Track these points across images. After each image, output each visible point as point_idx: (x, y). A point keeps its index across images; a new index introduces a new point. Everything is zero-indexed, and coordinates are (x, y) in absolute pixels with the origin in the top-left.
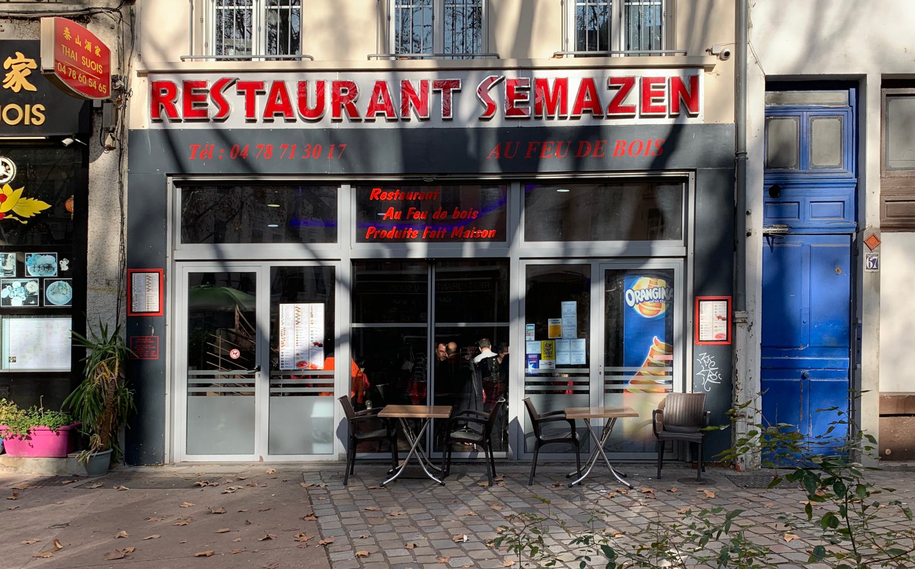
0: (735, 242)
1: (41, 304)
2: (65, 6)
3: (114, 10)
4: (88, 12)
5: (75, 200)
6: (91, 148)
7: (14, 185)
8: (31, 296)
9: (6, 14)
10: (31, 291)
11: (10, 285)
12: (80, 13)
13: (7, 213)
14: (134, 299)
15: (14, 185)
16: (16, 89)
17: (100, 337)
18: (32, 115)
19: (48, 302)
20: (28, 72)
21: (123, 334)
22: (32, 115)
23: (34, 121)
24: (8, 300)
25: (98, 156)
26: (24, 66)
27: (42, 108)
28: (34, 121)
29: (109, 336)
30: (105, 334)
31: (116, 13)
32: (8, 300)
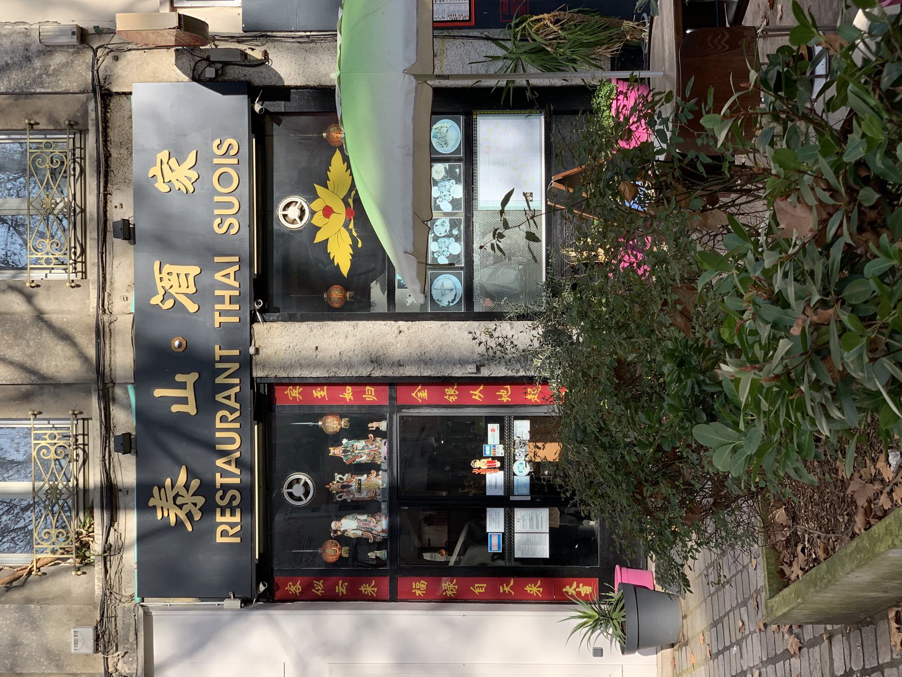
0: (525, 108)
1: (459, 160)
2: (90, 122)
3: (95, 55)
4: (98, 88)
5: (339, 518)
6: (266, 82)
7: (312, 196)
8: (450, 174)
9: (101, 195)
10: (443, 174)
11: (436, 199)
12: (99, 99)
13: (347, 204)
14: (453, 18)
15: (312, 196)
16: (194, 175)
17: (500, 64)
18: (223, 218)
19: (457, 151)
20: (173, 162)
21: (495, 33)
22: (223, 218)
23: (233, 152)
24: (454, 202)
25: (276, 74)
26: (165, 166)
27: (217, 142)
28: (233, 152)
29: (500, 52)
30: (495, 58)
31: (99, 53)
32: (454, 202)
